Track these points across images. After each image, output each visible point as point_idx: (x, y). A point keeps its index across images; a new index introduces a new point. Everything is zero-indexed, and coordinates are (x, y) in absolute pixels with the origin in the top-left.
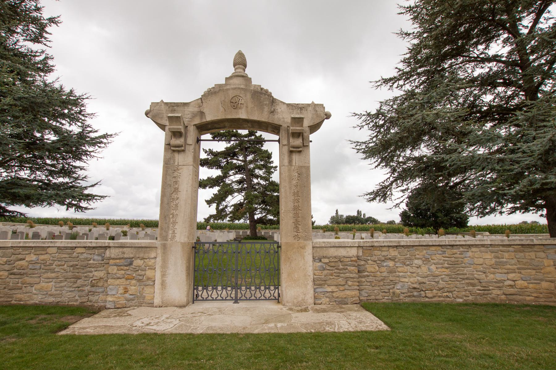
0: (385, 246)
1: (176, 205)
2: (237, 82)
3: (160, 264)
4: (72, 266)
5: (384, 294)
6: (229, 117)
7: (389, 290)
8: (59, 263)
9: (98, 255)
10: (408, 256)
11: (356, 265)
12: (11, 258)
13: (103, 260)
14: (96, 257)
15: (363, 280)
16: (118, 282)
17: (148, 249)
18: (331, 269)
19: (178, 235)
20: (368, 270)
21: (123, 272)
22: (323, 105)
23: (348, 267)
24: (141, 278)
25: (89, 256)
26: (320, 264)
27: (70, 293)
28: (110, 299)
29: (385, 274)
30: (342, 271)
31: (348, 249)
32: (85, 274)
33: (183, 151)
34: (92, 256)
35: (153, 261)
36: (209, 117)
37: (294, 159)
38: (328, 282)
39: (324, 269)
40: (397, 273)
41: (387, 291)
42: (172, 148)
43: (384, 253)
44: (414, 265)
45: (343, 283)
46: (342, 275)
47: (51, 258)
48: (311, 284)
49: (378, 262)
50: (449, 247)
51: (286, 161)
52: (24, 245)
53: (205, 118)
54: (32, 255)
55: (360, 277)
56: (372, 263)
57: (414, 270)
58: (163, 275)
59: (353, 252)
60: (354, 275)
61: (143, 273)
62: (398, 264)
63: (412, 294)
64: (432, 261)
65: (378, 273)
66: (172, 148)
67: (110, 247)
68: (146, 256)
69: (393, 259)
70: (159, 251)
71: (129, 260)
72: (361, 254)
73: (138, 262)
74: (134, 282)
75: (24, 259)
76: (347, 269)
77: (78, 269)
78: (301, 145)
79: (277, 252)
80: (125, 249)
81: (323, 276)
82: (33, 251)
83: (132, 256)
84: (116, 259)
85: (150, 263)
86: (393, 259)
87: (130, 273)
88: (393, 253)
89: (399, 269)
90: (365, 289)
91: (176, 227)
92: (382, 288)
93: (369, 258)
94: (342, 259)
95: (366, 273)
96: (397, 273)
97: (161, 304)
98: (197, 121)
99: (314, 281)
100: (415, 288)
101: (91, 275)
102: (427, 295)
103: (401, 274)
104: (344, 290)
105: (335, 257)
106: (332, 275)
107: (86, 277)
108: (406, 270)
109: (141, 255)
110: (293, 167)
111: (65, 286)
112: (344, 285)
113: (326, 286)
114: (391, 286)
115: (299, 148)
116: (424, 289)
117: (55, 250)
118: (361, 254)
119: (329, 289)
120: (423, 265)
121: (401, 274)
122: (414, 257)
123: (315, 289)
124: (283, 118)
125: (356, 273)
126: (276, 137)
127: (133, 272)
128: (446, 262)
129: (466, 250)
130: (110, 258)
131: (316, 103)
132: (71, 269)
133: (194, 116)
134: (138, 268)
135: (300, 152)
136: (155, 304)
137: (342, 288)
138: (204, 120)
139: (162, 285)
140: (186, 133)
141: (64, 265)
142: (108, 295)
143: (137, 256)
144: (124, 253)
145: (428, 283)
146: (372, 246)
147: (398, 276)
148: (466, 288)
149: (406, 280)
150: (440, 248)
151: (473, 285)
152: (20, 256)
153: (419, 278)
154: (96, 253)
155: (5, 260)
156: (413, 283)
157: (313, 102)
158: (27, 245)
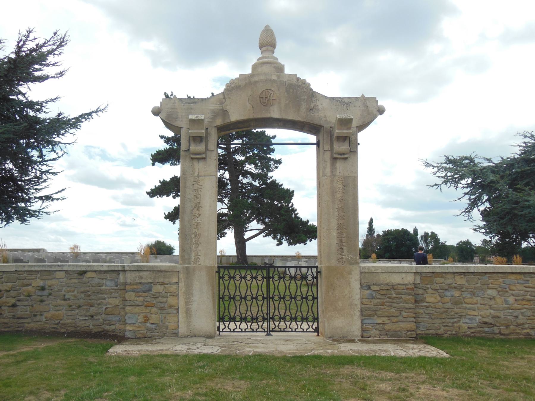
0: (449, 273)
1: (199, 223)
2: (265, 69)
3: (183, 291)
4: (83, 292)
6: (259, 116)
7: (453, 323)
8: (69, 289)
9: (111, 280)
10: (479, 285)
11: (413, 294)
12: (16, 284)
13: (117, 286)
14: (109, 283)
15: (421, 311)
16: (137, 309)
17: (168, 273)
18: (382, 297)
19: (202, 258)
20: (428, 299)
21: (142, 299)
22: (375, 98)
23: (403, 296)
24: (162, 305)
25: (101, 281)
26: (368, 292)
27: (83, 322)
28: (128, 328)
29: (449, 305)
31: (404, 275)
32: (99, 302)
33: (204, 159)
34: (104, 281)
35: (174, 287)
36: (234, 117)
37: (338, 168)
38: (377, 313)
39: (373, 298)
40: (464, 305)
41: (450, 324)
42: (192, 156)
43: (449, 281)
44: (486, 296)
45: (396, 314)
46: (395, 305)
47: (60, 284)
48: (358, 314)
49: (440, 291)
51: (328, 171)
52: (29, 269)
53: (229, 118)
54: (38, 280)
55: (417, 307)
56: (433, 292)
57: (487, 301)
58: (188, 302)
59: (410, 279)
60: (410, 305)
61: (165, 300)
62: (466, 295)
63: (482, 329)
64: (510, 292)
65: (440, 304)
66: (192, 156)
67: (125, 271)
68: (166, 281)
69: (459, 288)
70: (181, 276)
71: (147, 286)
72: (418, 281)
74: (154, 310)
75: (30, 285)
76: (401, 298)
77: (90, 295)
78: (349, 151)
79: (316, 278)
80: (142, 274)
81: (372, 306)
82: (39, 275)
83: (150, 281)
84: (133, 284)
85: (172, 289)
86: (459, 288)
87: (149, 300)
88: (460, 281)
90: (423, 321)
91: (199, 248)
92: (444, 321)
93: (429, 286)
94: (396, 287)
95: (425, 304)
97: (186, 334)
98: (219, 122)
99: (361, 311)
100: (486, 323)
102: (502, 332)
103: (468, 306)
104: (397, 322)
105: (387, 284)
106: (383, 304)
107: (99, 304)
108: (475, 301)
109: (161, 280)
110: (337, 178)
111: (78, 314)
112: (397, 316)
113: (376, 317)
114: (455, 320)
115: (344, 154)
116: (498, 325)
117: (63, 274)
118: (418, 281)
119: (379, 321)
120: (498, 296)
121: (468, 306)
122: (486, 287)
123: (362, 320)
124: (325, 117)
125: (412, 303)
126: (313, 138)
127: (153, 299)
128: (529, 293)
130: (125, 284)
131: (366, 96)
132: (83, 295)
133: (216, 114)
134: (158, 295)
135: (346, 159)
136: (180, 334)
137: (395, 320)
138: (227, 121)
139: (187, 313)
140: (207, 137)
141: (73, 291)
142: (127, 323)
143: (157, 281)
144: (141, 278)
145: (503, 317)
146: (433, 273)
147: (465, 308)
149: (475, 313)
150: (522, 276)
152: (26, 282)
153: (492, 311)
154: (109, 278)
155: (11, 286)
156: (483, 317)
157: (363, 95)
158: (33, 269)
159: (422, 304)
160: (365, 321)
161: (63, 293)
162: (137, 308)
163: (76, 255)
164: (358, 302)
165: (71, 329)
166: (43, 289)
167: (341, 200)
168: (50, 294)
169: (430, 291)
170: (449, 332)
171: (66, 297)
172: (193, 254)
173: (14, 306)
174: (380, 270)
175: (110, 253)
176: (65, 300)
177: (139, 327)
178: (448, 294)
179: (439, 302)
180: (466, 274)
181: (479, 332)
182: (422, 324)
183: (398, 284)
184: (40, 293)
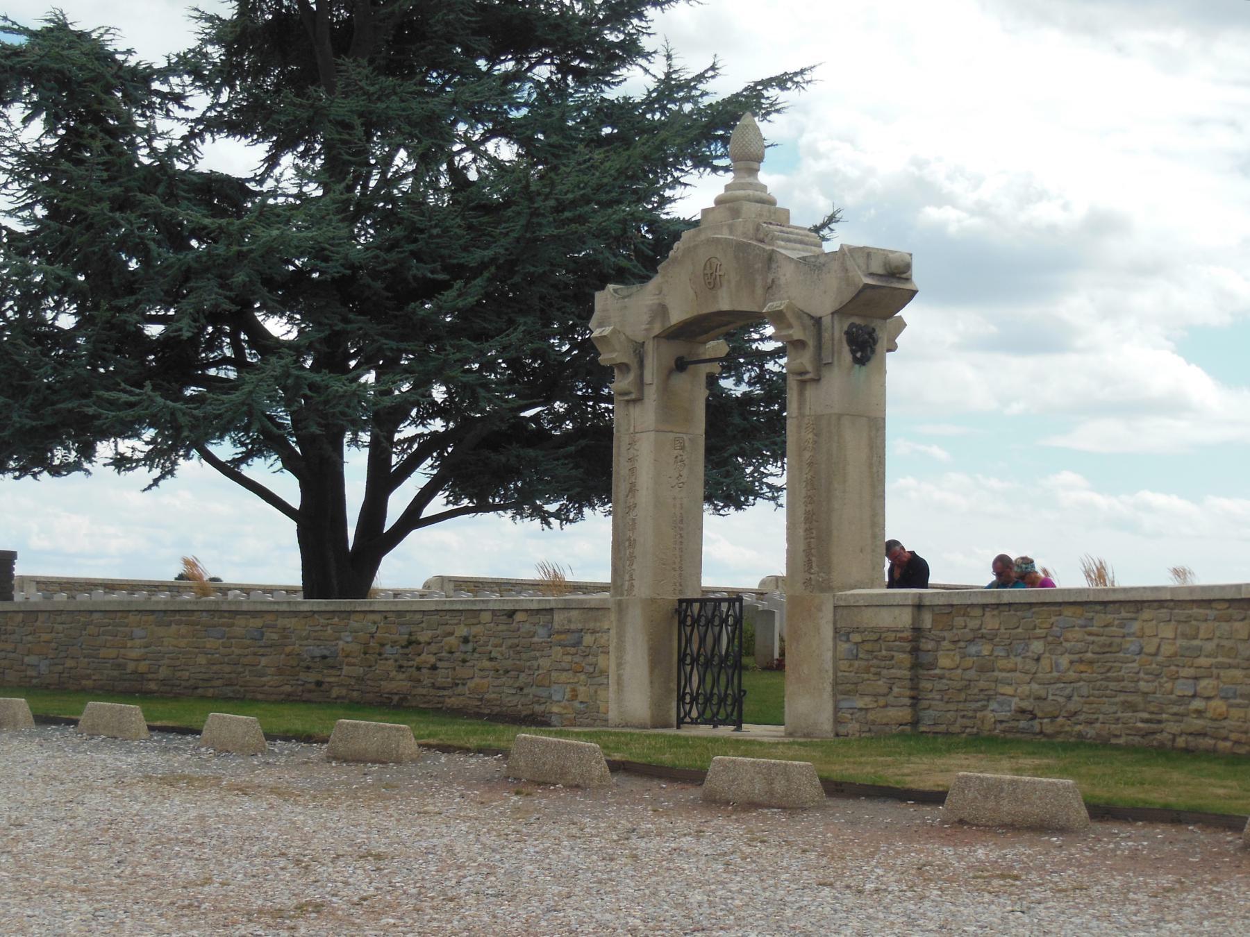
5: (965, 721)
7: (975, 711)
12: (438, 632)
17: (600, 613)
29: (972, 674)
30: (883, 664)
31: (897, 611)
36: (677, 317)
44: (1030, 654)
48: (829, 689)
50: (1098, 608)
58: (619, 665)
69: (990, 638)
70: (613, 616)
73: (588, 639)
74: (583, 677)
77: (519, 653)
83: (580, 626)
86: (990, 638)
89: (1001, 663)
92: (961, 706)
93: (946, 634)
95: (937, 671)
96: (996, 674)
98: (657, 329)
99: (836, 683)
101: (535, 664)
106: (867, 671)
114: (979, 704)
119: (860, 704)
129: (1129, 615)
137: (882, 701)
148: (1119, 714)
149: (1009, 690)
151: (1133, 708)
152: (448, 629)
159: (932, 672)
160: (844, 704)
161: (490, 648)
162: (565, 673)
163: (556, 585)
164: (829, 666)
165: (496, 710)
166: (466, 640)
167: (810, 464)
168: (474, 650)
169: (945, 644)
170: (968, 730)
171: (493, 655)
172: (627, 577)
173: (434, 668)
174: (861, 603)
175: (956, 588)
176: (491, 659)
177: (565, 708)
178: (973, 649)
179: (957, 668)
180: (1001, 608)
181: (1010, 730)
182: (931, 712)
183: (889, 630)
184: (463, 648)
